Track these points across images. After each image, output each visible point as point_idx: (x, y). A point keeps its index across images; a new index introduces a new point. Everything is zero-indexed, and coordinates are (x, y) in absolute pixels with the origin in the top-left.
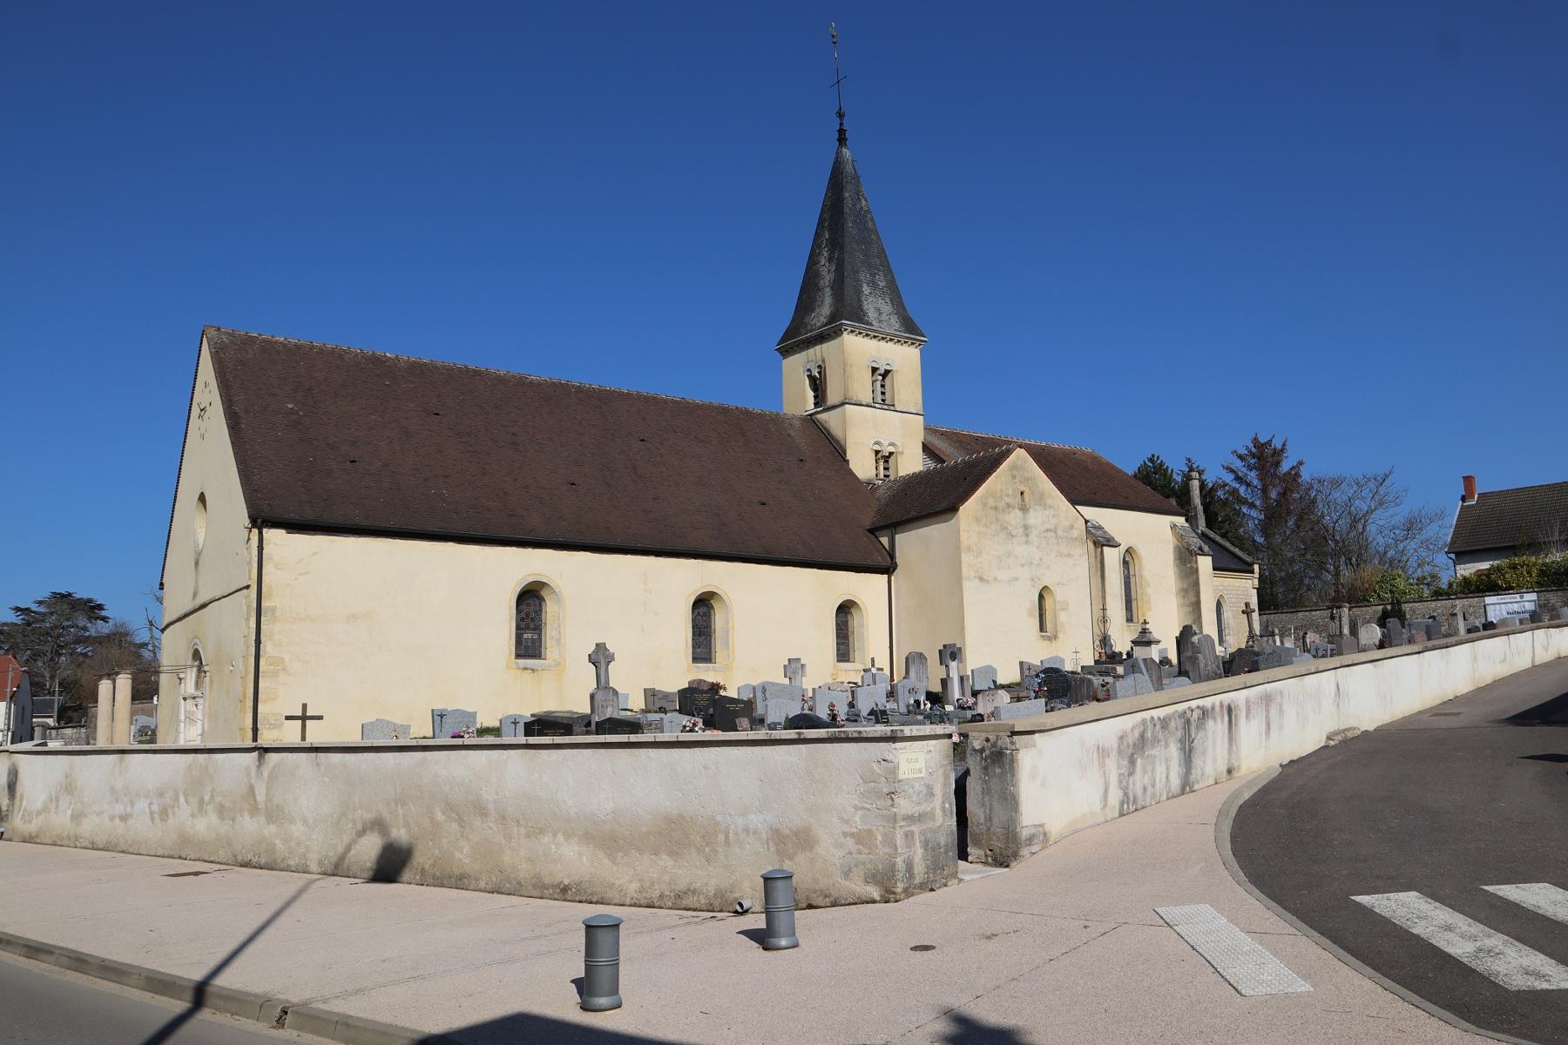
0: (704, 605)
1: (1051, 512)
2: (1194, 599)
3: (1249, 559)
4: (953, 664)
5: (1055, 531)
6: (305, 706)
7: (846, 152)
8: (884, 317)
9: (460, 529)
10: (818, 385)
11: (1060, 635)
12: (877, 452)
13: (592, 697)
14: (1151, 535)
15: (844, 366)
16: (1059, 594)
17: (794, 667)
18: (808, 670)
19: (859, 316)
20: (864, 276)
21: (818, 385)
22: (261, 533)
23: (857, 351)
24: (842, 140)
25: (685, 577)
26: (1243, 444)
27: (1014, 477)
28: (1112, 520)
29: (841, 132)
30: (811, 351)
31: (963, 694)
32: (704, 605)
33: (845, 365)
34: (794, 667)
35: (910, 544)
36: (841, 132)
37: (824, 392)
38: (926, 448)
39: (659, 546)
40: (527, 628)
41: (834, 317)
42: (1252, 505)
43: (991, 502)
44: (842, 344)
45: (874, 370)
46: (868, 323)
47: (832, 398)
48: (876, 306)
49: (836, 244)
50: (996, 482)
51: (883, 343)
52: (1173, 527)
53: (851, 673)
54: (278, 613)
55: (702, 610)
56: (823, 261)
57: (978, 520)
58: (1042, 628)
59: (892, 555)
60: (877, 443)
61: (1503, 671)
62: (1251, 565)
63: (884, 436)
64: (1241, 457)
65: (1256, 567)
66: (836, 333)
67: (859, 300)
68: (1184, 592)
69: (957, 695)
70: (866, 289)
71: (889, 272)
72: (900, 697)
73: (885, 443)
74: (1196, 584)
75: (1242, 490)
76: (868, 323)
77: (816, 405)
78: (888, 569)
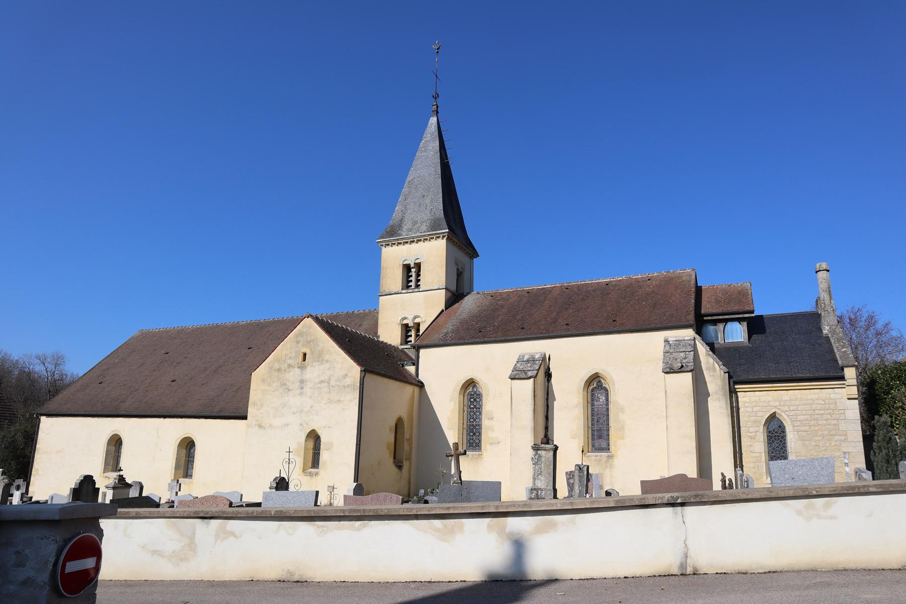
1: (327, 365)
31: (738, 462)
32: (188, 446)
43: (276, 366)
50: (287, 349)
57: (264, 381)
61: (167, 571)
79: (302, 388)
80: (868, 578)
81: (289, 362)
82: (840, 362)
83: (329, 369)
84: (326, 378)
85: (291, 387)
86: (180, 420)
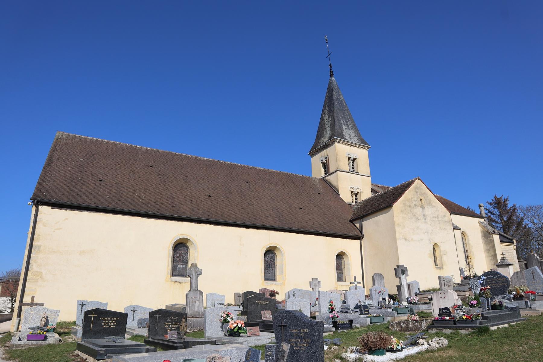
0: (270, 253)
2: (493, 253)
3: (511, 238)
4: (403, 277)
5: (438, 218)
6: (33, 298)
7: (333, 79)
8: (352, 137)
9: (145, 210)
10: (326, 166)
11: (444, 267)
12: (352, 192)
13: (187, 295)
14: (473, 226)
15: (336, 156)
16: (442, 247)
17: (315, 283)
18: (322, 284)
19: (341, 136)
20: (343, 122)
21: (326, 166)
22: (37, 208)
23: (341, 151)
24: (331, 75)
25: (265, 238)
26: (491, 199)
27: (417, 192)
28: (458, 219)
29: (331, 72)
30: (323, 152)
31: (410, 295)
32: (270, 253)
33: (337, 155)
34: (315, 283)
35: (369, 225)
36: (331, 72)
37: (328, 168)
38: (373, 190)
39: (247, 223)
40: (180, 262)
41: (331, 137)
42: (497, 222)
43: (407, 203)
44: (335, 147)
45: (349, 158)
46: (345, 139)
47: (332, 169)
48: (348, 133)
49: (331, 111)
51: (352, 147)
52: (480, 223)
53: (344, 286)
54: (42, 248)
55: (271, 255)
56: (326, 118)
58: (436, 264)
59: (361, 232)
60: (352, 188)
62: (512, 240)
63: (354, 184)
64: (491, 204)
65: (514, 241)
66: (333, 143)
67: (341, 131)
68: (488, 251)
69: (407, 296)
70: (344, 127)
71: (353, 121)
72: (374, 297)
73: (355, 188)
74: (494, 247)
75: (492, 216)
76: (345, 139)
77: (325, 174)
78: (359, 238)
79: (425, 219)
80: (483, 338)
81: (414, 202)
82: (188, 271)
83: (436, 211)
84: (436, 216)
85: (419, 218)
86: (265, 231)
